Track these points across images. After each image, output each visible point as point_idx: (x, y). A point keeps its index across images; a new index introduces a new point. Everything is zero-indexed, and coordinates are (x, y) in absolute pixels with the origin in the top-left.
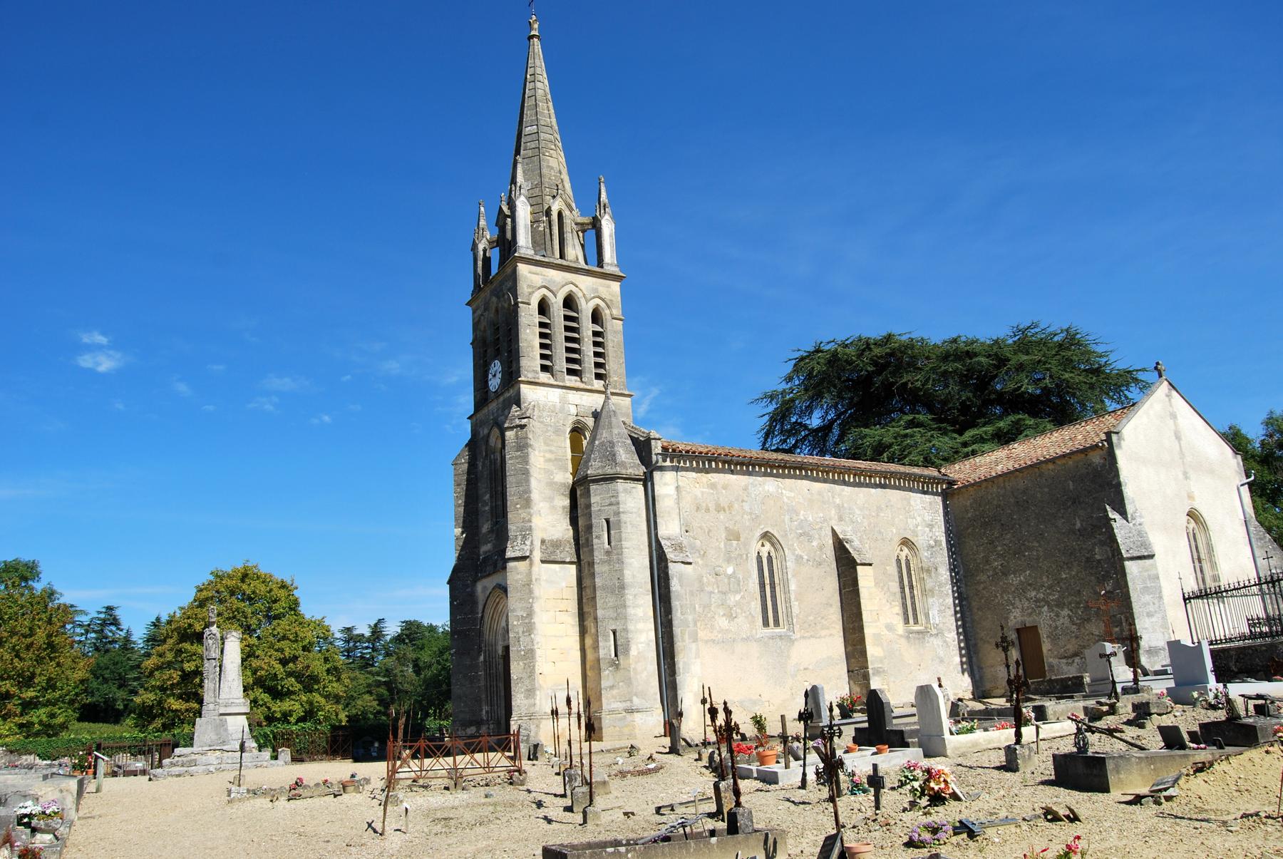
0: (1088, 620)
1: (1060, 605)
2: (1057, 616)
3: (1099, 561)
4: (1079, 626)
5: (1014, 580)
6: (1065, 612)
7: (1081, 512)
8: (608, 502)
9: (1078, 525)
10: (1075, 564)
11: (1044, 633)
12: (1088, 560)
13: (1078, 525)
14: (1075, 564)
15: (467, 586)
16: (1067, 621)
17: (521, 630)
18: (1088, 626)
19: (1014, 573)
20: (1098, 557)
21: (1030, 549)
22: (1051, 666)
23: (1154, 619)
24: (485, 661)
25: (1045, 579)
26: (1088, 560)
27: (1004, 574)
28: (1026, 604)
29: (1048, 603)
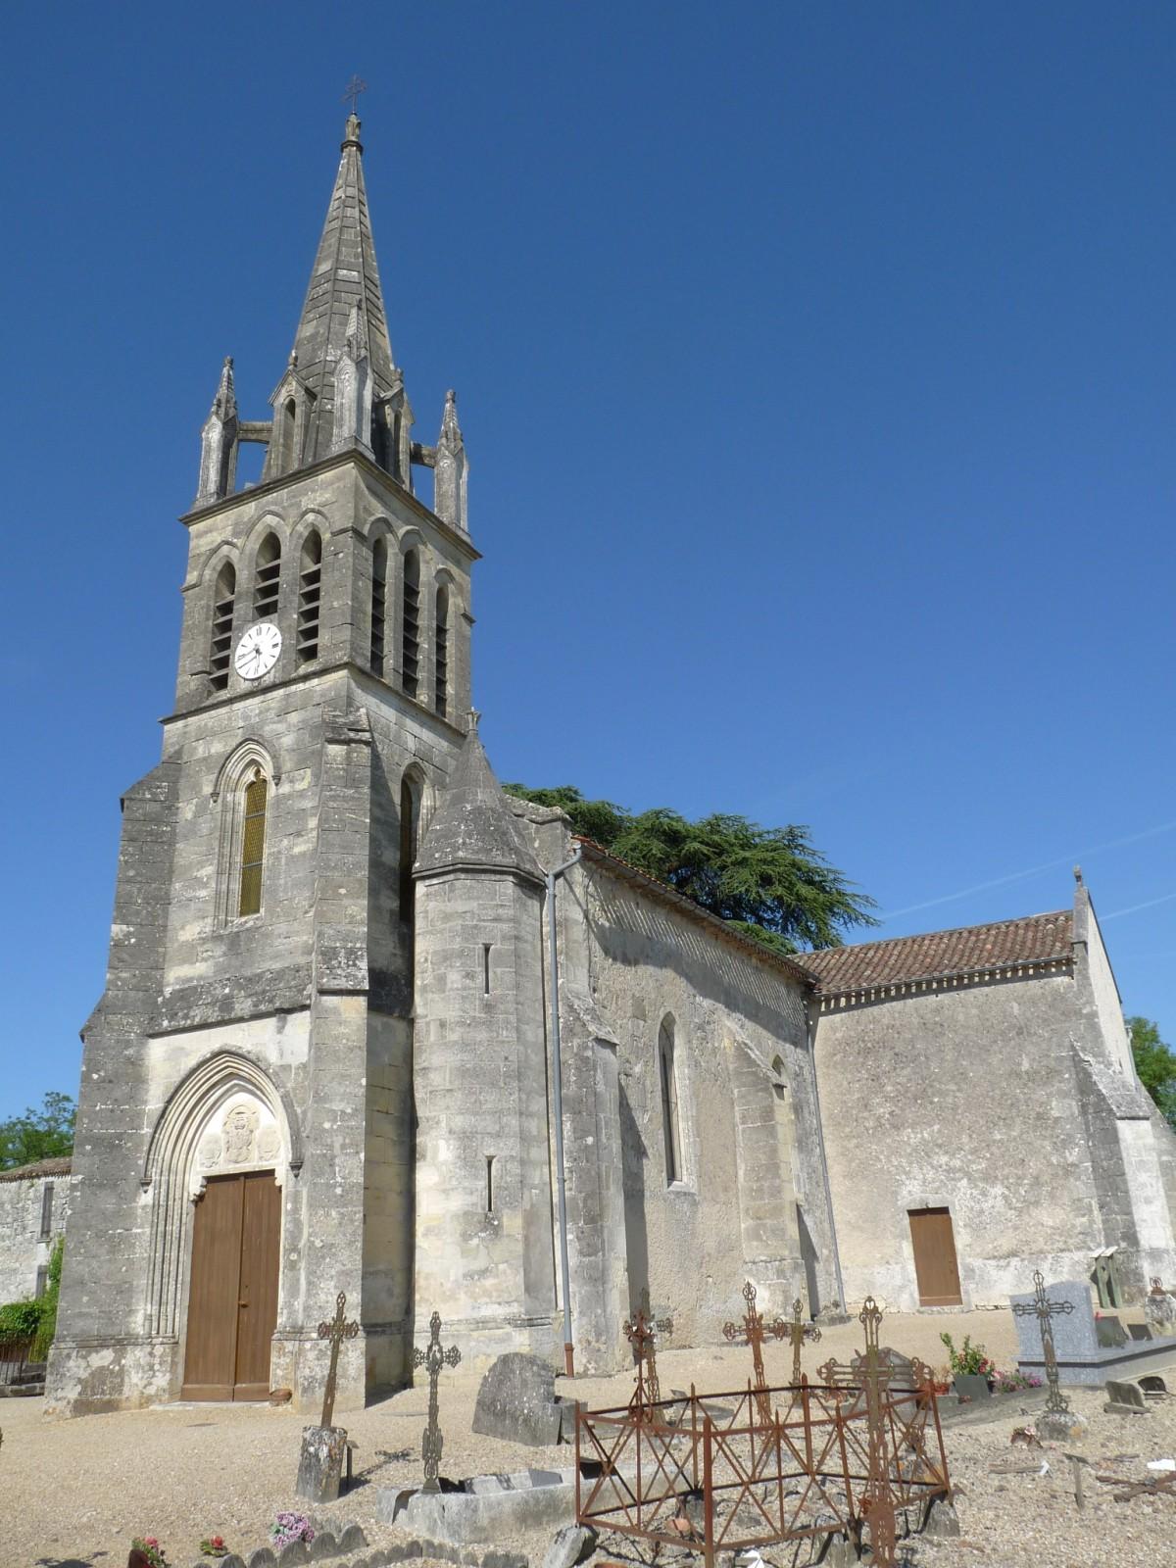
0: (1037, 1203)
1: (989, 1178)
2: (984, 1194)
3: (1057, 1120)
4: (1020, 1212)
5: (912, 1137)
6: (998, 1190)
7: (1030, 1048)
8: (492, 914)
9: (1025, 1066)
10: (1018, 1120)
11: (958, 1218)
12: (1039, 1117)
13: (1025, 1066)
14: (1018, 1120)
15: (128, 1044)
16: (1000, 1202)
17: (338, 1141)
18: (1034, 1212)
19: (913, 1126)
20: (1055, 1113)
21: (942, 1094)
22: (970, 1271)
23: (1153, 1208)
24: (156, 1206)
25: (965, 1139)
26: (1039, 1117)
27: (896, 1127)
28: (930, 1175)
29: (969, 1176)
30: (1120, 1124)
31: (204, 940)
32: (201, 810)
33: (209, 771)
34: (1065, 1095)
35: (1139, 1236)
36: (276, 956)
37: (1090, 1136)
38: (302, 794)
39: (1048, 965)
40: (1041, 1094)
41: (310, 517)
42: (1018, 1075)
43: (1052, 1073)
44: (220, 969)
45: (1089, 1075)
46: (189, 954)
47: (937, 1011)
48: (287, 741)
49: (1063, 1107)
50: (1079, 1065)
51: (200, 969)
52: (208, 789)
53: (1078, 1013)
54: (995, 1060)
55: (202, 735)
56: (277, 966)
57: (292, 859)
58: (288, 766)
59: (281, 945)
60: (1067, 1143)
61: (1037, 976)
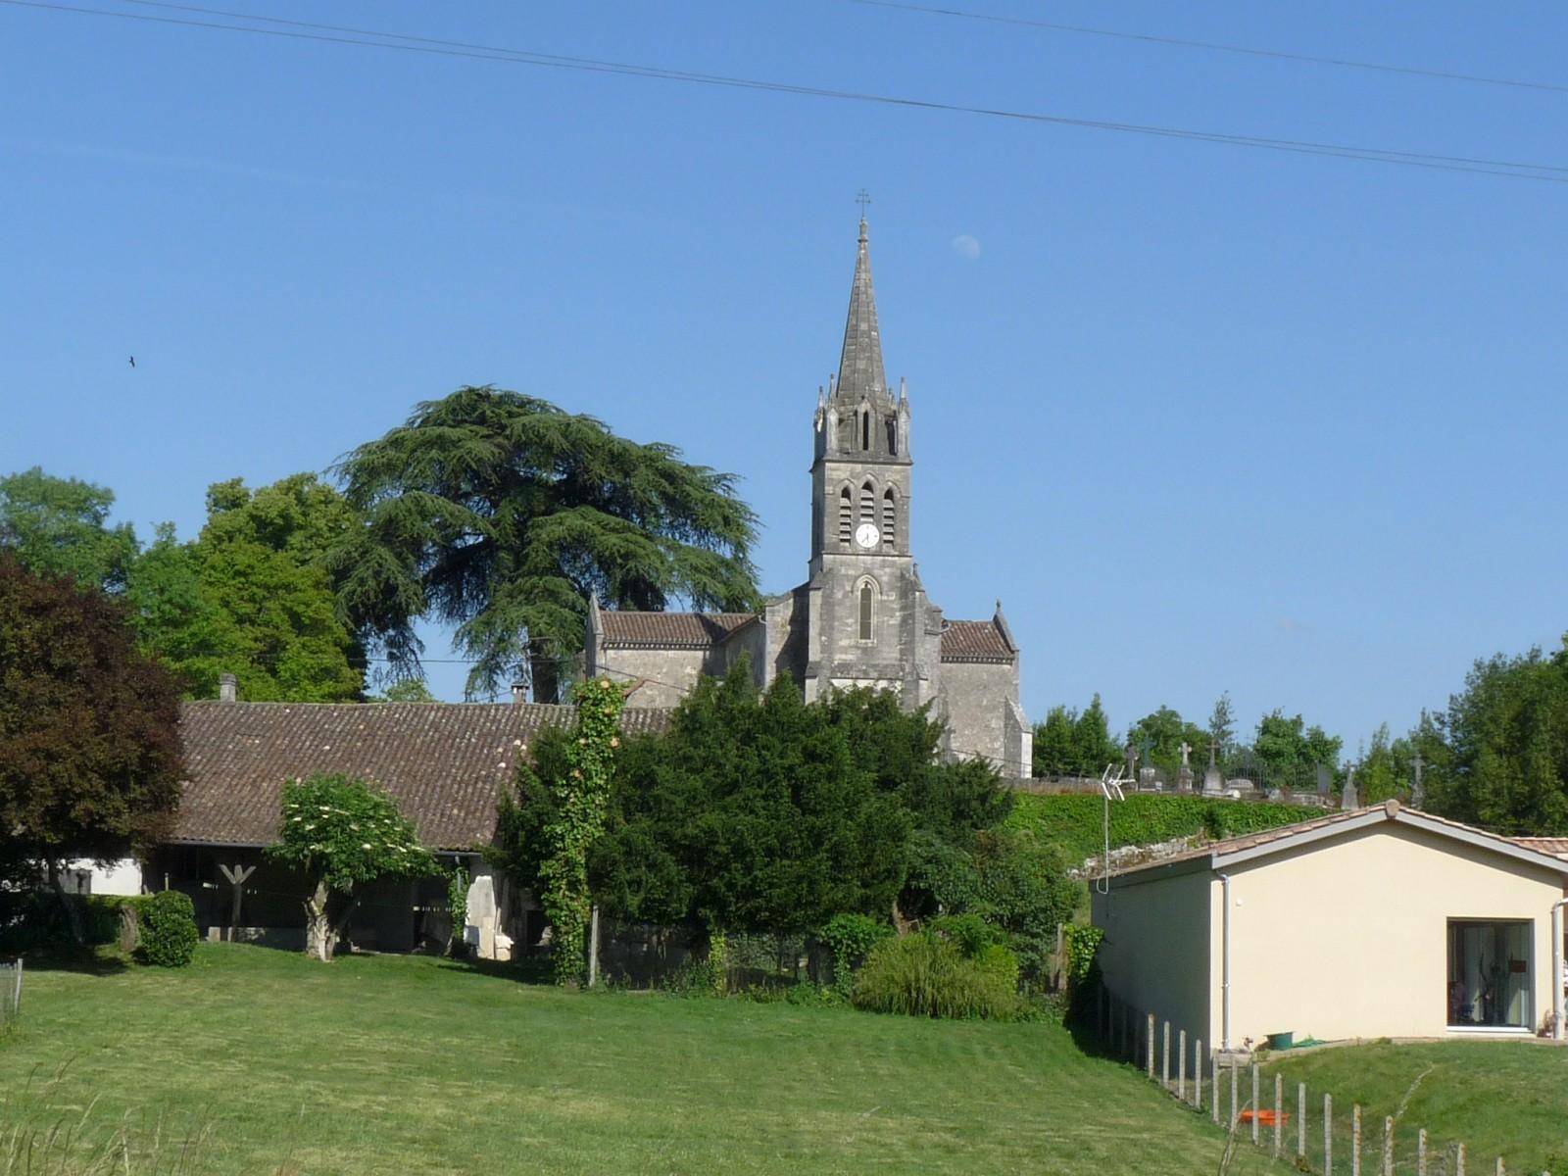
9: (985, 703)
12: (986, 726)
26: (986, 726)
30: (1024, 735)
31: (851, 647)
32: (845, 595)
33: (848, 580)
34: (998, 718)
35: (120, 975)
36: (884, 659)
37: (1006, 737)
38: (892, 601)
39: (1002, 659)
40: (989, 716)
41: (890, 484)
42: (980, 706)
43: (995, 708)
44: (858, 659)
45: (1012, 711)
46: (844, 650)
47: (949, 671)
48: (885, 579)
49: (997, 724)
50: (1007, 705)
51: (850, 657)
52: (848, 589)
53: (1011, 683)
54: (971, 699)
55: (848, 565)
56: (885, 662)
57: (889, 625)
58: (885, 589)
59: (885, 655)
60: (996, 739)
61: (997, 663)
